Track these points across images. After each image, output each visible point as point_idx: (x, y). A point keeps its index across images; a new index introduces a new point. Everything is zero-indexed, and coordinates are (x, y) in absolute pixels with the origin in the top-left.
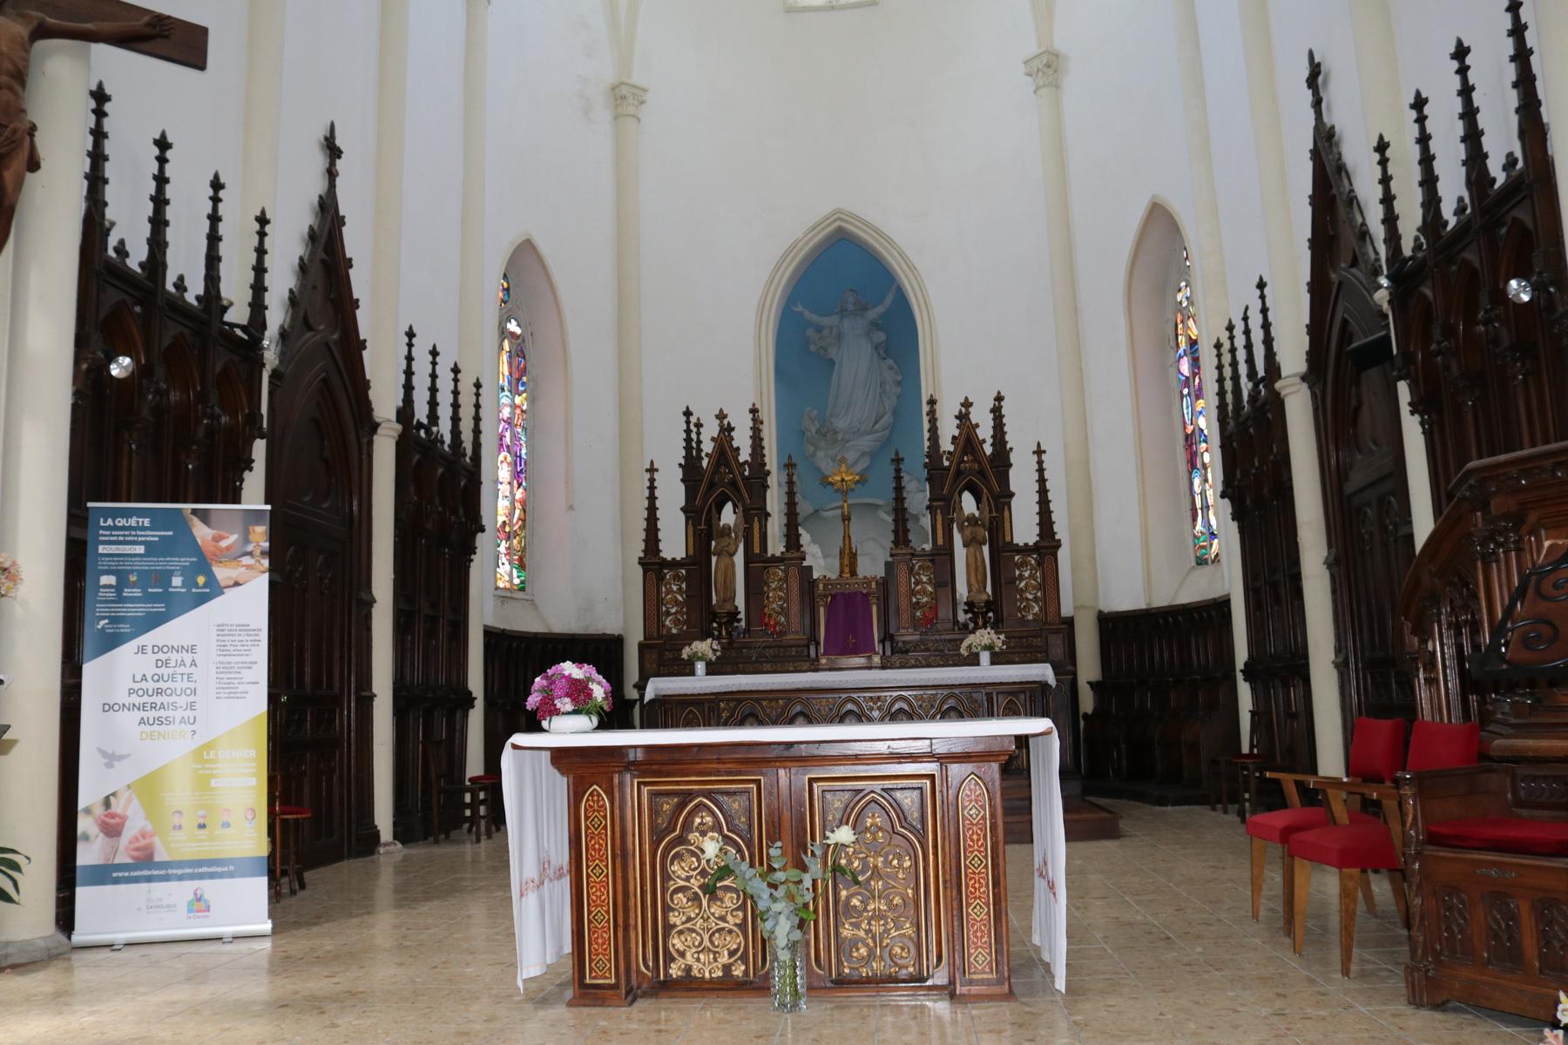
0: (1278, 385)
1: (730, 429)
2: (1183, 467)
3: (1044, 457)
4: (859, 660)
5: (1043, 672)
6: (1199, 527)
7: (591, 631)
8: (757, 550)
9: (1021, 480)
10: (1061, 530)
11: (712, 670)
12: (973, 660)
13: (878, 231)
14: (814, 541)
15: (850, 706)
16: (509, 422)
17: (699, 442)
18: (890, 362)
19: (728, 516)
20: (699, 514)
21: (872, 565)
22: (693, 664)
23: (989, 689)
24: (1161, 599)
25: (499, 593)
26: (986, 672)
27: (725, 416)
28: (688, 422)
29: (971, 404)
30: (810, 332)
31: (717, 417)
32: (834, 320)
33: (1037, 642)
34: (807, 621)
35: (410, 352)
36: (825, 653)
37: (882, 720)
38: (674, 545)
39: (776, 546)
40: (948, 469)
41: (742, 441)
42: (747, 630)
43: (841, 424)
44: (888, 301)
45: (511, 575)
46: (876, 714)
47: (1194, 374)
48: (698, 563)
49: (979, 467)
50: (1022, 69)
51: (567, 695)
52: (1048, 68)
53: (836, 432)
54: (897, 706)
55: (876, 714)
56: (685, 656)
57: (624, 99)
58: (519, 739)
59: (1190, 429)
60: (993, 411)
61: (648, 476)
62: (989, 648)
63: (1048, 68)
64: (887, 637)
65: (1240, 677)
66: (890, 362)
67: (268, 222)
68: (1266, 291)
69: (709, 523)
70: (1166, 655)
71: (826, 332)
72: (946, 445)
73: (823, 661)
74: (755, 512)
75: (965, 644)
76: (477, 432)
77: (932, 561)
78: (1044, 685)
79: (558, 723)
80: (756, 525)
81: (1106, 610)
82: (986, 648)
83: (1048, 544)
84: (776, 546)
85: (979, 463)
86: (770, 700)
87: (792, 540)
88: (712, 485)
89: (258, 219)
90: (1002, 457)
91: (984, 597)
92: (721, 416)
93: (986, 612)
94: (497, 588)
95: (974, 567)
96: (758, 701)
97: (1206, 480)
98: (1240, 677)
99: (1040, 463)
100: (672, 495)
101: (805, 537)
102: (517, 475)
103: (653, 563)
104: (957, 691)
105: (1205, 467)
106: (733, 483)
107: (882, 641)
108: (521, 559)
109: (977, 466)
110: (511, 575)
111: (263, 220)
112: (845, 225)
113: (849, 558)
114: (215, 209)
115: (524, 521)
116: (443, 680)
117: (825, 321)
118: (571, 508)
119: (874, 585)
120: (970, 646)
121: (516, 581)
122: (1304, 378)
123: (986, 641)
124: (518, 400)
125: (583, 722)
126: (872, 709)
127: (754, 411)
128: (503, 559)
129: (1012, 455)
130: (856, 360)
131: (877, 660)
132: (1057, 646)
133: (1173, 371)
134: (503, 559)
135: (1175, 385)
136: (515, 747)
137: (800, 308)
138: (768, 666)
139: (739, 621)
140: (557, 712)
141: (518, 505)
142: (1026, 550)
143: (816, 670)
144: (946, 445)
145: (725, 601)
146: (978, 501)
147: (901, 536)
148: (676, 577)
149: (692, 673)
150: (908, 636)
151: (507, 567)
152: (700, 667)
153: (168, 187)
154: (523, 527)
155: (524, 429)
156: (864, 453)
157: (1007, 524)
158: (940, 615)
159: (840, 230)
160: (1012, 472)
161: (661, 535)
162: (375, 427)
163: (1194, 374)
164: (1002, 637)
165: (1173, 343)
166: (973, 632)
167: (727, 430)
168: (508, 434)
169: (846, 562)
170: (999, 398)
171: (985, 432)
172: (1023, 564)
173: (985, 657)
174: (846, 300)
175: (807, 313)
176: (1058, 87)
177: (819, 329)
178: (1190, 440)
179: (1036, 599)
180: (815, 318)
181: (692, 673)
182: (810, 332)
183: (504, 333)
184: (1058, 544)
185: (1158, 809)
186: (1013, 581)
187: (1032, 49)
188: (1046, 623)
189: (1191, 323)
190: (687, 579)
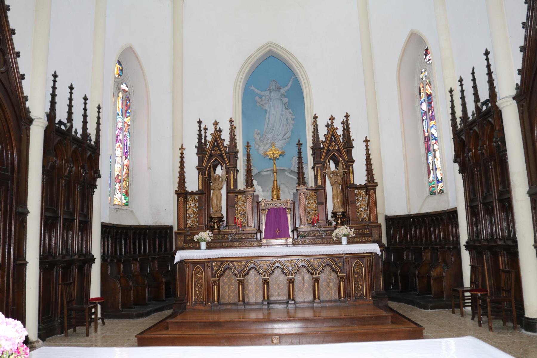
1: (220, 131)
4: (281, 241)
6: (431, 177)
7: (159, 224)
8: (232, 187)
9: (358, 154)
11: (209, 247)
13: (287, 51)
14: (259, 184)
15: (277, 264)
16: (121, 129)
17: (206, 137)
18: (290, 110)
19: (219, 171)
20: (205, 172)
21: (287, 195)
22: (200, 243)
24: (415, 210)
25: (115, 207)
27: (218, 124)
28: (200, 127)
29: (334, 119)
31: (214, 124)
32: (267, 93)
33: (367, 231)
34: (256, 221)
35: (54, 84)
36: (265, 238)
38: (193, 184)
39: (241, 185)
40: (323, 149)
41: (226, 136)
42: (227, 225)
47: (429, 110)
49: (335, 148)
53: (268, 140)
56: (195, 240)
59: (427, 134)
61: (180, 152)
62: (347, 235)
64: (295, 229)
66: (290, 110)
67: (87, 99)
68: (489, 56)
69: (209, 174)
71: (263, 98)
72: (322, 138)
73: (264, 241)
74: (232, 169)
76: (98, 130)
80: (232, 175)
81: (389, 214)
82: (345, 235)
84: (241, 185)
86: (238, 261)
87: (249, 183)
88: (211, 156)
89: (69, 88)
90: (348, 144)
92: (216, 124)
93: (342, 218)
94: (114, 205)
96: (231, 262)
97: (435, 157)
99: (367, 146)
100: (192, 160)
101: (255, 182)
102: (125, 153)
103: (182, 194)
105: (435, 151)
106: (221, 155)
107: (293, 231)
108: (126, 192)
110: (121, 199)
111: (55, 76)
112: (272, 48)
113: (277, 192)
114: (71, 96)
115: (128, 174)
116: (76, 249)
117: (263, 93)
118: (150, 168)
119: (289, 204)
121: (124, 201)
122: (514, 98)
123: (345, 232)
124: (126, 120)
127: (231, 121)
128: (117, 191)
131: (290, 241)
133: (418, 109)
134: (117, 191)
135: (419, 115)
137: (253, 88)
138: (237, 244)
139: (223, 221)
141: (125, 167)
142: (360, 187)
145: (216, 211)
146: (337, 164)
148: (194, 200)
149: (199, 248)
150: (304, 228)
151: (119, 195)
152: (203, 245)
153: (56, 90)
154: (127, 177)
155: (129, 133)
157: (351, 175)
159: (270, 51)
162: (31, 121)
163: (429, 110)
164: (353, 230)
166: (336, 228)
168: (121, 135)
169: (275, 193)
170: (347, 116)
171: (340, 132)
172: (359, 194)
173: (344, 240)
174: (273, 78)
175: (256, 90)
180: (259, 92)
181: (199, 248)
182: (257, 98)
183: (119, 89)
185: (423, 310)
186: (354, 202)
188: (370, 222)
189: (428, 87)
190: (199, 201)
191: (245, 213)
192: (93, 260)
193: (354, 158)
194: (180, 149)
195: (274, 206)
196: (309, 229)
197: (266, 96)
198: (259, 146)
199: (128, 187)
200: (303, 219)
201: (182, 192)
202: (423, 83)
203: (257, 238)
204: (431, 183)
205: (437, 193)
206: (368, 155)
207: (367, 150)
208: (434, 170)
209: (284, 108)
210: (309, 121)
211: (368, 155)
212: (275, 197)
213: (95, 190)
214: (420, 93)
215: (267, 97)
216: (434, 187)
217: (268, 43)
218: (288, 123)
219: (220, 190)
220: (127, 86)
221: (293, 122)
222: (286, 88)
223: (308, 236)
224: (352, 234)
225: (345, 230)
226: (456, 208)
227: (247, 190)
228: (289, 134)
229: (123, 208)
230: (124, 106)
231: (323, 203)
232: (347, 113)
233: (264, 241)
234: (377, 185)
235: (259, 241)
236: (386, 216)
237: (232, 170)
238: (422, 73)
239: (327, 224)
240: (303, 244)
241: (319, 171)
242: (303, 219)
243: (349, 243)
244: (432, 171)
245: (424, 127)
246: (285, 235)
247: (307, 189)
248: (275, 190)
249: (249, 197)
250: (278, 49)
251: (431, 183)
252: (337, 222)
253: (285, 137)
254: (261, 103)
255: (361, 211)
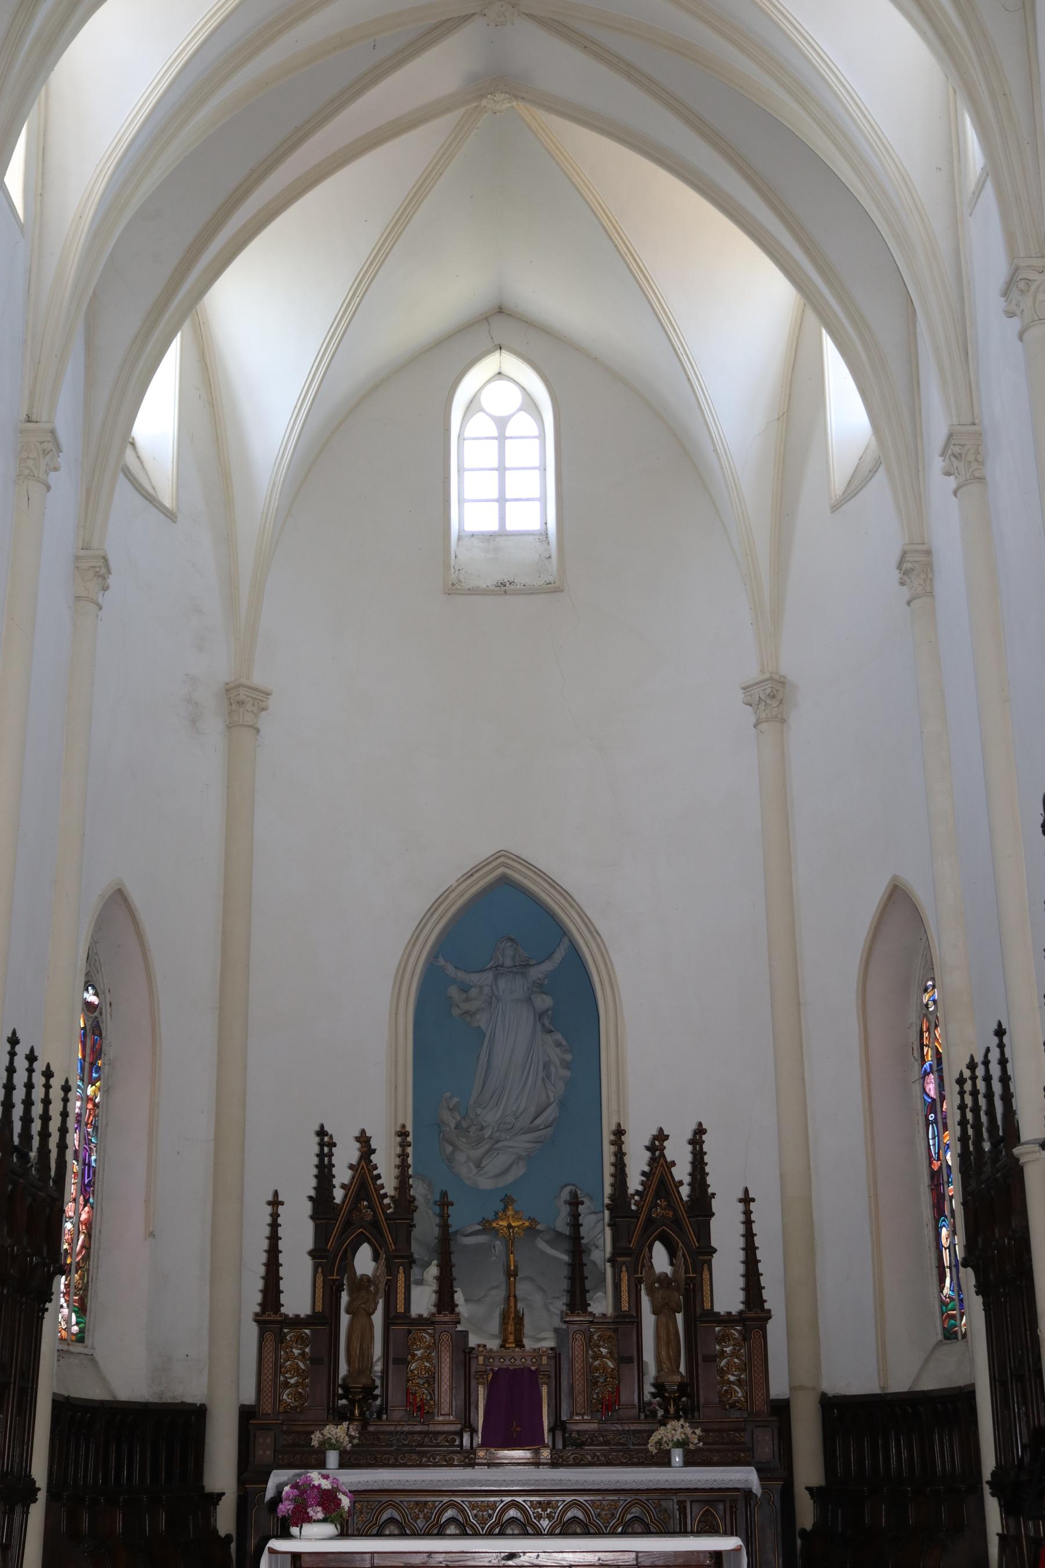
0: (1016, 1151)
2: (927, 1212)
3: (753, 1206)
5: (746, 1477)
7: (167, 1398)
8: (401, 1309)
9: (725, 1231)
10: (773, 1297)
12: (663, 1460)
15: (512, 1513)
21: (540, 1338)
22: (324, 1453)
23: (682, 1497)
24: (900, 1383)
26: (678, 1474)
30: (453, 991)
32: (488, 976)
36: (486, 1444)
37: (551, 1534)
38: (298, 1297)
40: (636, 1215)
43: (490, 1117)
44: (558, 957)
45: (68, 1321)
46: (545, 1523)
48: (324, 1318)
50: (740, 695)
51: (318, 1505)
52: (771, 698)
53: (482, 1129)
54: (569, 1515)
55: (545, 1523)
56: (315, 1443)
57: (242, 704)
58: (276, 1544)
59: (936, 1166)
60: (692, 1142)
62: (682, 1444)
63: (771, 698)
64: (558, 1425)
65: (987, 1490)
66: (559, 1036)
70: (905, 1454)
71: (474, 992)
72: (634, 1183)
73: (481, 1453)
75: (655, 1437)
77: (616, 1330)
78: (748, 1493)
79: (309, 1529)
80: (401, 1277)
82: (679, 1444)
83: (755, 1311)
84: (422, 1300)
85: (675, 1211)
87: (445, 1301)
88: (348, 1224)
90: (701, 1202)
91: (677, 1379)
93: (679, 1399)
95: (665, 1336)
98: (987, 1490)
101: (459, 1297)
104: (643, 1497)
106: (375, 1224)
107: (552, 1430)
109: (670, 1211)
112: (509, 872)
113: (513, 1323)
117: (475, 977)
118: (152, 1235)
120: (659, 1442)
121: (75, 1329)
123: (678, 1436)
125: (330, 1529)
126: (539, 1517)
129: (714, 1203)
130: (513, 1037)
131: (546, 1454)
132: (766, 1446)
133: (917, 1087)
135: (919, 1106)
136: (272, 1551)
140: (310, 1520)
141: (82, 1228)
142: (728, 1320)
143: (472, 1465)
144: (634, 1183)
147: (577, 1299)
148: (301, 1340)
150: (584, 1424)
151: (65, 1311)
152: (332, 1458)
156: (519, 1158)
157: (706, 1288)
158: (624, 1398)
159: (504, 881)
160: (713, 1222)
161: (283, 1285)
164: (698, 1431)
165: (917, 1054)
166: (663, 1423)
167: (366, 1148)
169: (511, 1328)
170: (700, 1131)
171: (682, 1172)
172: (723, 1339)
174: (509, 962)
176: (783, 721)
177: (464, 989)
178: (937, 1180)
179: (739, 1382)
180: (461, 975)
182: (453, 991)
184: (767, 1315)
187: (752, 673)
191: (431, 1379)
192: (30, 1493)
193: (713, 1244)
194: (269, 1203)
195: (508, 1362)
196: (594, 1426)
197: (481, 988)
198: (455, 1147)
199: (85, 1288)
200: (580, 1399)
201: (273, 1317)
202: (928, 1020)
203: (461, 1445)
204: (947, 1305)
205: (960, 1337)
206: (749, 1236)
207: (748, 1223)
208: (954, 1269)
209: (539, 1027)
210: (607, 1137)
211: (749, 1236)
212: (511, 1338)
213: (48, 1305)
214: (922, 1046)
215: (486, 990)
216: (953, 1317)
217: (497, 855)
218: (548, 1076)
219: (370, 1314)
220: (96, 994)
221: (567, 1073)
222: (548, 966)
223: (591, 1445)
224: (696, 1441)
225: (680, 1430)
226: (973, 1385)
227: (440, 1318)
228: (551, 1113)
229: (71, 1349)
230: (88, 1051)
231: (632, 1358)
232: (700, 1124)
233: (481, 1453)
234: (770, 1318)
235: (467, 1451)
236: (824, 1395)
237: (402, 1264)
238: (926, 990)
239: (642, 1416)
240: (578, 1463)
241: (625, 1276)
242: (580, 1399)
243: (687, 1463)
244: (948, 1271)
245: (931, 1142)
246: (528, 1439)
247: (591, 1322)
248: (511, 1322)
249: (445, 1337)
250: (526, 876)
251: (947, 1305)
252: (667, 1411)
253: (538, 1122)
254: (466, 1006)
255: (730, 1382)
